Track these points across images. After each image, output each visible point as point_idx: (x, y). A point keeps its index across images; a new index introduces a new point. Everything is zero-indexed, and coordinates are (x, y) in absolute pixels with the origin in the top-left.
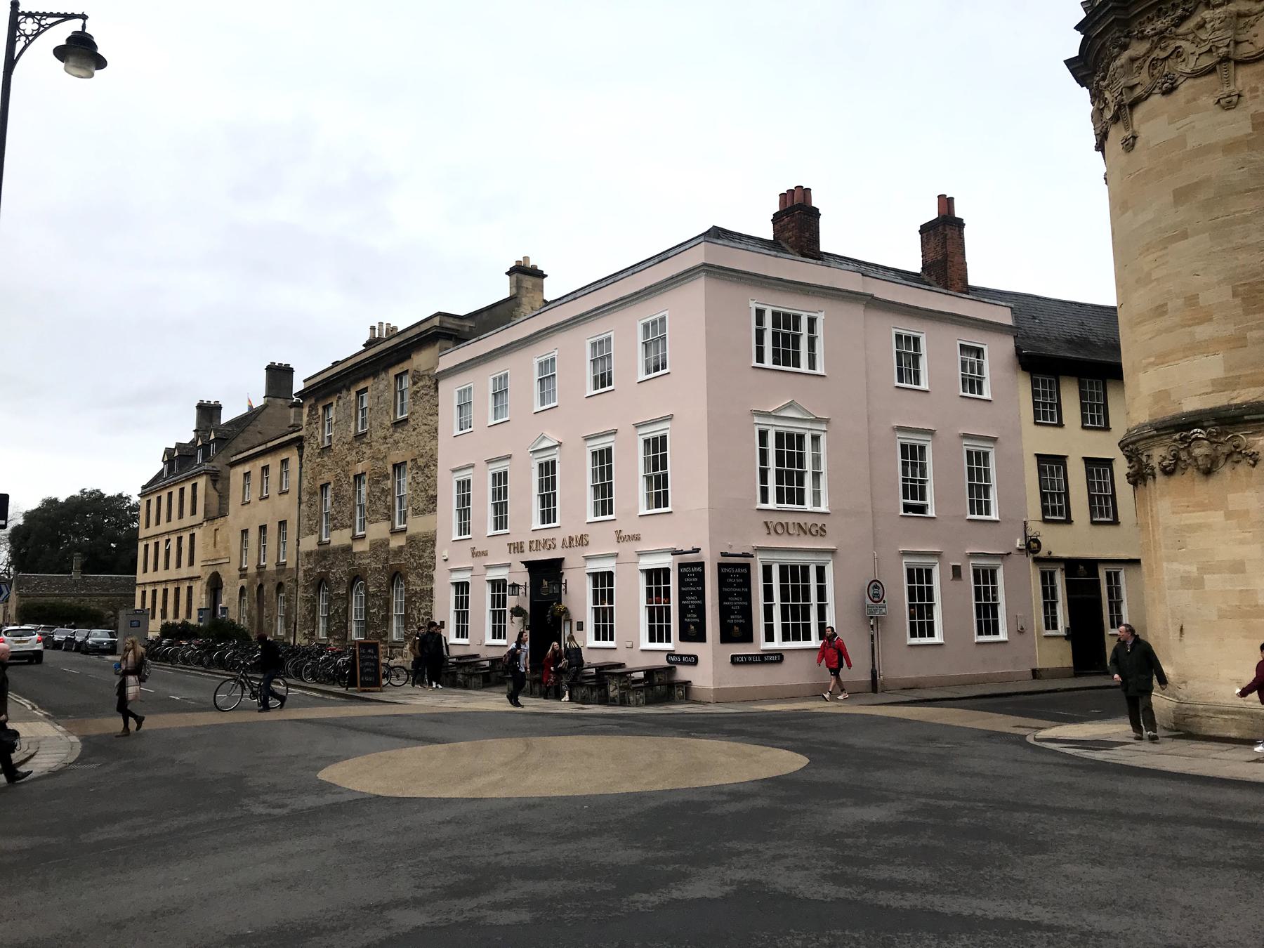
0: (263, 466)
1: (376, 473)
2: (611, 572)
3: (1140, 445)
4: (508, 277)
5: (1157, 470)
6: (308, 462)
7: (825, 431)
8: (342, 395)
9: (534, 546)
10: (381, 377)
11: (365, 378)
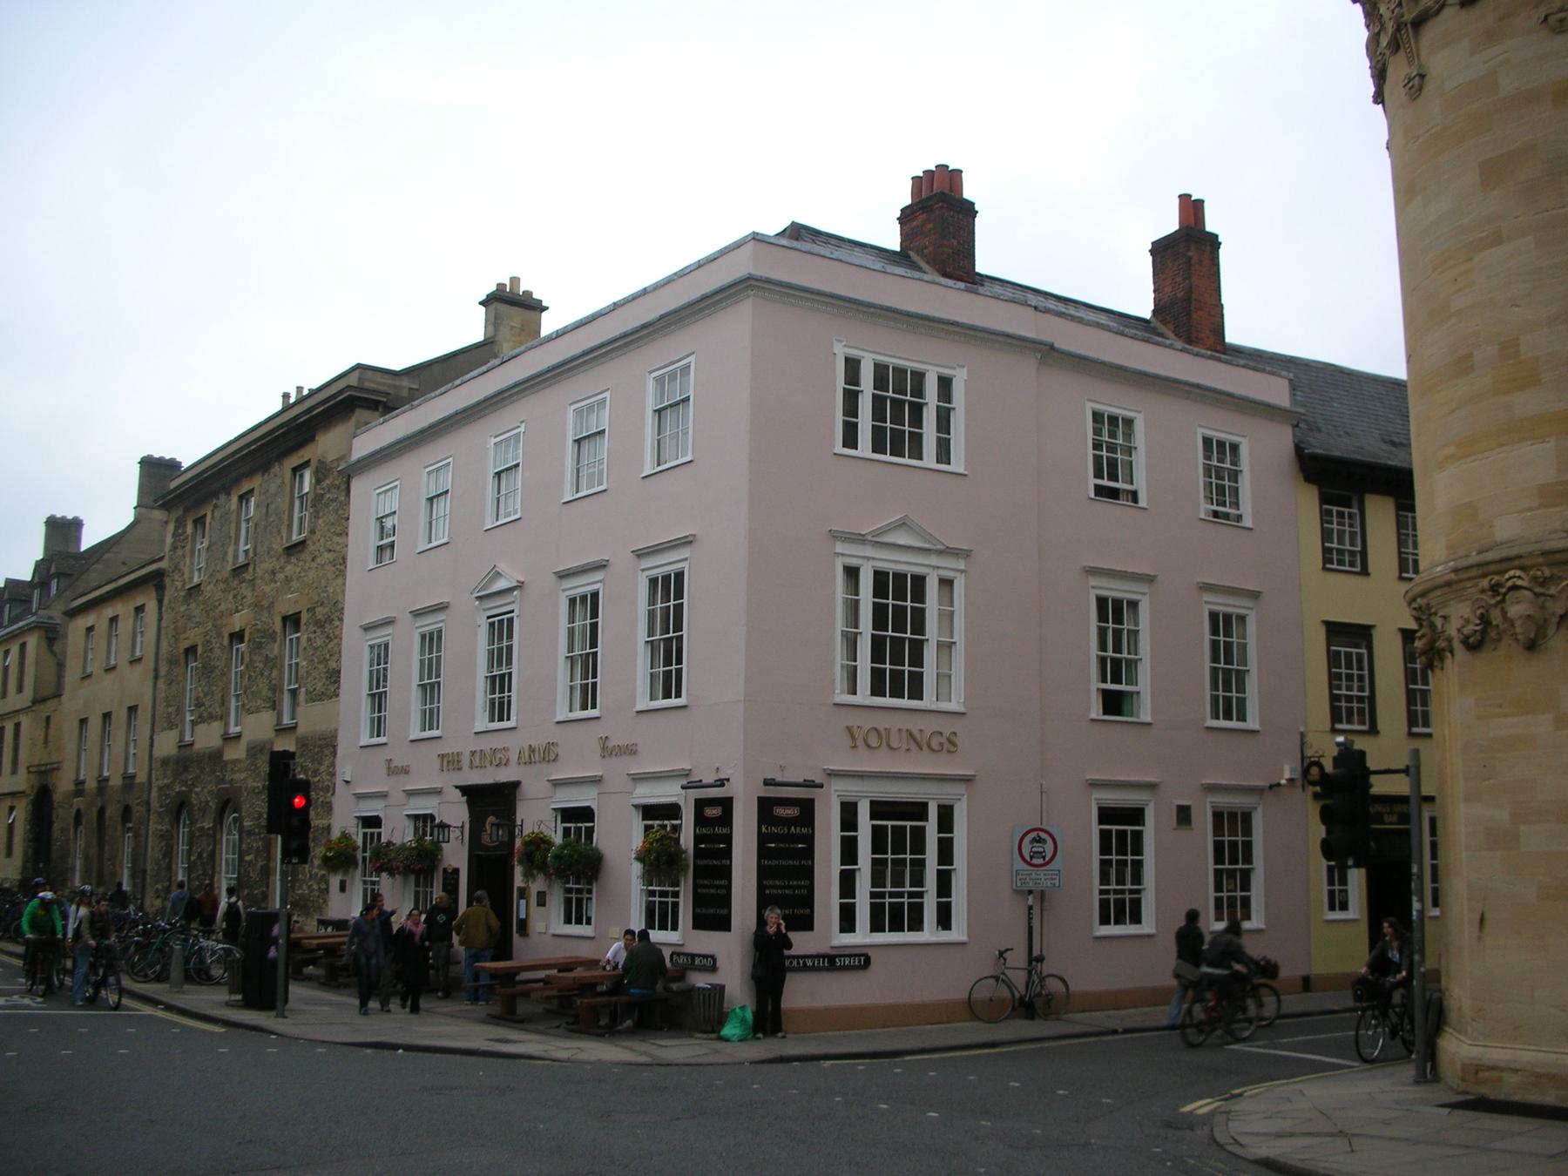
0: (110, 616)
1: (258, 631)
2: (589, 807)
3: (1434, 599)
4: (483, 309)
5: (1457, 645)
6: (169, 611)
7: (962, 571)
8: (219, 503)
9: (477, 762)
10: (273, 471)
11: (250, 474)
